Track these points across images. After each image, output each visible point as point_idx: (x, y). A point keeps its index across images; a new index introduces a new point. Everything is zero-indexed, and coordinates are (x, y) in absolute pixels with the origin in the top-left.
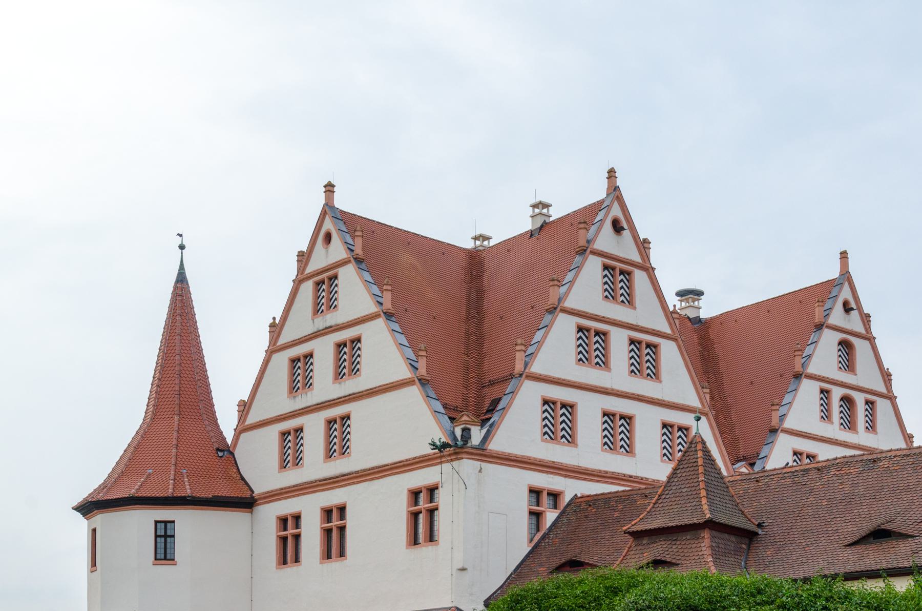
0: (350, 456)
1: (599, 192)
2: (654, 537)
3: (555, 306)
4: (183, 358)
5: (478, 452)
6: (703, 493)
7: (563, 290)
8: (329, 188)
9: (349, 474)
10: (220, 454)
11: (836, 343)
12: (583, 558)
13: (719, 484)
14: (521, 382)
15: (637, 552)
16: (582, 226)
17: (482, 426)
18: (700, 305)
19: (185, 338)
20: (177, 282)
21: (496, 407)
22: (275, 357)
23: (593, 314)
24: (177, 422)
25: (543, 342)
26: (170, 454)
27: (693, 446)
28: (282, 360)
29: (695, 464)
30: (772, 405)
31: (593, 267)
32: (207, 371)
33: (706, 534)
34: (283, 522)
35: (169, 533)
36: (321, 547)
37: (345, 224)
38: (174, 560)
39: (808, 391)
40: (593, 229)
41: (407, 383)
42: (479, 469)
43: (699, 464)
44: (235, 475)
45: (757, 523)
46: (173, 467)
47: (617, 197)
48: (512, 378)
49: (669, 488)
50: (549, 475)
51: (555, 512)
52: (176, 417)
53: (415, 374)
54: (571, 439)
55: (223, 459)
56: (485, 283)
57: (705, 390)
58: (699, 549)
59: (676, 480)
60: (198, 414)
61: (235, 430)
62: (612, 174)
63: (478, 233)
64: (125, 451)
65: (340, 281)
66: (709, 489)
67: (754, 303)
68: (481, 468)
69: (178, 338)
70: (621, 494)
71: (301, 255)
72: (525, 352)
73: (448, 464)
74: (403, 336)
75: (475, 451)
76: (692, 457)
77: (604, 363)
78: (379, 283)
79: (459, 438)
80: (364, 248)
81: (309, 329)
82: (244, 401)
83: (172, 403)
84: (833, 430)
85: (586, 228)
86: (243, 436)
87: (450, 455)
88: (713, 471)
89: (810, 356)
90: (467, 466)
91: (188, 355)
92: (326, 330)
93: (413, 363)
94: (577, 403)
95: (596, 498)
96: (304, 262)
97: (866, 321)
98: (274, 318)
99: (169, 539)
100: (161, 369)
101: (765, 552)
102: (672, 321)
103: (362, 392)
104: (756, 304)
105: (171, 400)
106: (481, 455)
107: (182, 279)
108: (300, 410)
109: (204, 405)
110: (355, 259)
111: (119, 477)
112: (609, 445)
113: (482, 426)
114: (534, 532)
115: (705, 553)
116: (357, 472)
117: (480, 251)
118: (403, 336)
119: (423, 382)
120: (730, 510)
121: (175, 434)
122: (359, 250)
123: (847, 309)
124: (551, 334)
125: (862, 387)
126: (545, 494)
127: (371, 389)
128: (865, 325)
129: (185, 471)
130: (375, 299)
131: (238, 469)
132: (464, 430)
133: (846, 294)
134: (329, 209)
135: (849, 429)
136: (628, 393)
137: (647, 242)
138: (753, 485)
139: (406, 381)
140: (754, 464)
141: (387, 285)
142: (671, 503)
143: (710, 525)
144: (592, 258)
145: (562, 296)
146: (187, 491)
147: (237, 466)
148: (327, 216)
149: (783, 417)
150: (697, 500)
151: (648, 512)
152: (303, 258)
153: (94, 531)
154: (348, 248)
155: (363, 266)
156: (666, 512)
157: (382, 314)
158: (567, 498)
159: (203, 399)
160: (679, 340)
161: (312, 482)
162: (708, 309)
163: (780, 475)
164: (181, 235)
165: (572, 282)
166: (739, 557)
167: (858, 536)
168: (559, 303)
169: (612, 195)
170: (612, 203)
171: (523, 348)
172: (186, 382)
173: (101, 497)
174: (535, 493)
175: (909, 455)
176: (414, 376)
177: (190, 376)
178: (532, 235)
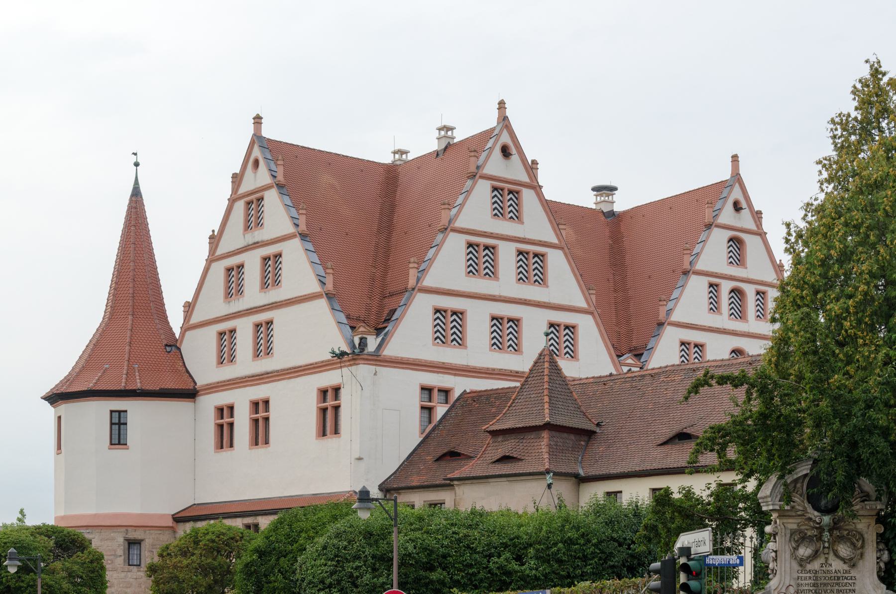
0: (273, 356)
1: (491, 121)
2: (507, 436)
3: (446, 227)
4: (136, 265)
5: (373, 358)
6: (546, 399)
7: (454, 211)
8: (258, 120)
9: (271, 372)
10: (168, 349)
11: (726, 240)
12: (461, 450)
13: (564, 390)
14: (413, 295)
15: (493, 448)
16: (472, 154)
17: (378, 335)
18: (614, 200)
19: (138, 246)
20: (132, 195)
21: (391, 317)
22: (214, 265)
23: (481, 232)
24: (130, 322)
25: (435, 259)
26: (124, 351)
27: (542, 357)
28: (219, 268)
29: (542, 374)
30: (660, 301)
31: (482, 191)
32: (158, 274)
33: (545, 434)
34: (220, 411)
35: (122, 421)
36: (250, 434)
37: (270, 151)
38: (126, 444)
39: (696, 287)
40: (484, 155)
41: (316, 296)
42: (374, 372)
43: (545, 374)
44: (181, 369)
45: (596, 423)
46: (126, 363)
47: (506, 125)
48: (407, 291)
49: (521, 394)
50: (440, 375)
51: (446, 407)
52: (130, 317)
53: (323, 289)
54: (460, 341)
55: (171, 354)
56: (397, 197)
57: (591, 292)
58: (539, 447)
59: (527, 387)
60: (150, 314)
61: (181, 328)
62: (502, 105)
63: (397, 148)
64: (87, 346)
65: (265, 202)
66: (553, 395)
67: (660, 199)
68: (376, 372)
69: (132, 246)
70: (499, 392)
71: (235, 176)
72: (417, 268)
73: (346, 368)
74: (315, 254)
75: (370, 357)
76: (540, 368)
77: (492, 273)
78: (296, 206)
79: (357, 346)
80: (285, 176)
81: (241, 244)
82: (188, 302)
83: (127, 304)
84: (723, 320)
85: (475, 156)
86: (188, 334)
87: (349, 361)
88: (558, 379)
89: (698, 254)
90: (364, 370)
91: (141, 261)
92: (255, 245)
93: (322, 279)
94: (466, 310)
95: (480, 394)
96: (237, 183)
97: (757, 219)
98: (213, 231)
99: (122, 426)
100: (118, 273)
101: (598, 448)
102: (558, 232)
103: (282, 301)
104: (662, 200)
105: (126, 301)
106: (376, 360)
107: (136, 193)
108: (233, 314)
109: (155, 306)
110: (277, 185)
111: (80, 371)
112: (497, 344)
113: (378, 335)
114: (426, 424)
115: (544, 450)
116: (277, 371)
117: (397, 165)
118: (315, 255)
119: (329, 296)
120: (572, 412)
121: (129, 333)
122: (280, 177)
123: (737, 207)
124: (441, 252)
125: (752, 279)
126: (436, 391)
127: (289, 300)
128: (755, 222)
129: (137, 366)
130: (293, 221)
131: (184, 363)
132: (361, 339)
133: (736, 194)
134: (258, 139)
135: (741, 318)
136: (515, 299)
137: (535, 164)
138: (601, 387)
139: (317, 294)
140: (642, 354)
141: (302, 209)
142: (522, 407)
143: (548, 426)
144: (481, 182)
145: (452, 217)
146: (138, 385)
147: (183, 360)
148: (256, 145)
149: (669, 312)
150: (541, 405)
151: (504, 414)
152: (237, 179)
153: (59, 418)
154: (272, 175)
155: (284, 191)
156: (518, 414)
157: (298, 235)
158: (456, 394)
159: (154, 300)
160: (566, 248)
161: (242, 378)
162: (621, 203)
163: (623, 380)
164: (135, 154)
165: (462, 205)
166: (576, 453)
167: (668, 436)
168: (449, 224)
169: (501, 125)
170: (501, 131)
171: (416, 265)
172: (139, 286)
173: (64, 389)
174: (427, 390)
175: (720, 366)
176: (322, 291)
177: (142, 280)
178: (438, 155)
